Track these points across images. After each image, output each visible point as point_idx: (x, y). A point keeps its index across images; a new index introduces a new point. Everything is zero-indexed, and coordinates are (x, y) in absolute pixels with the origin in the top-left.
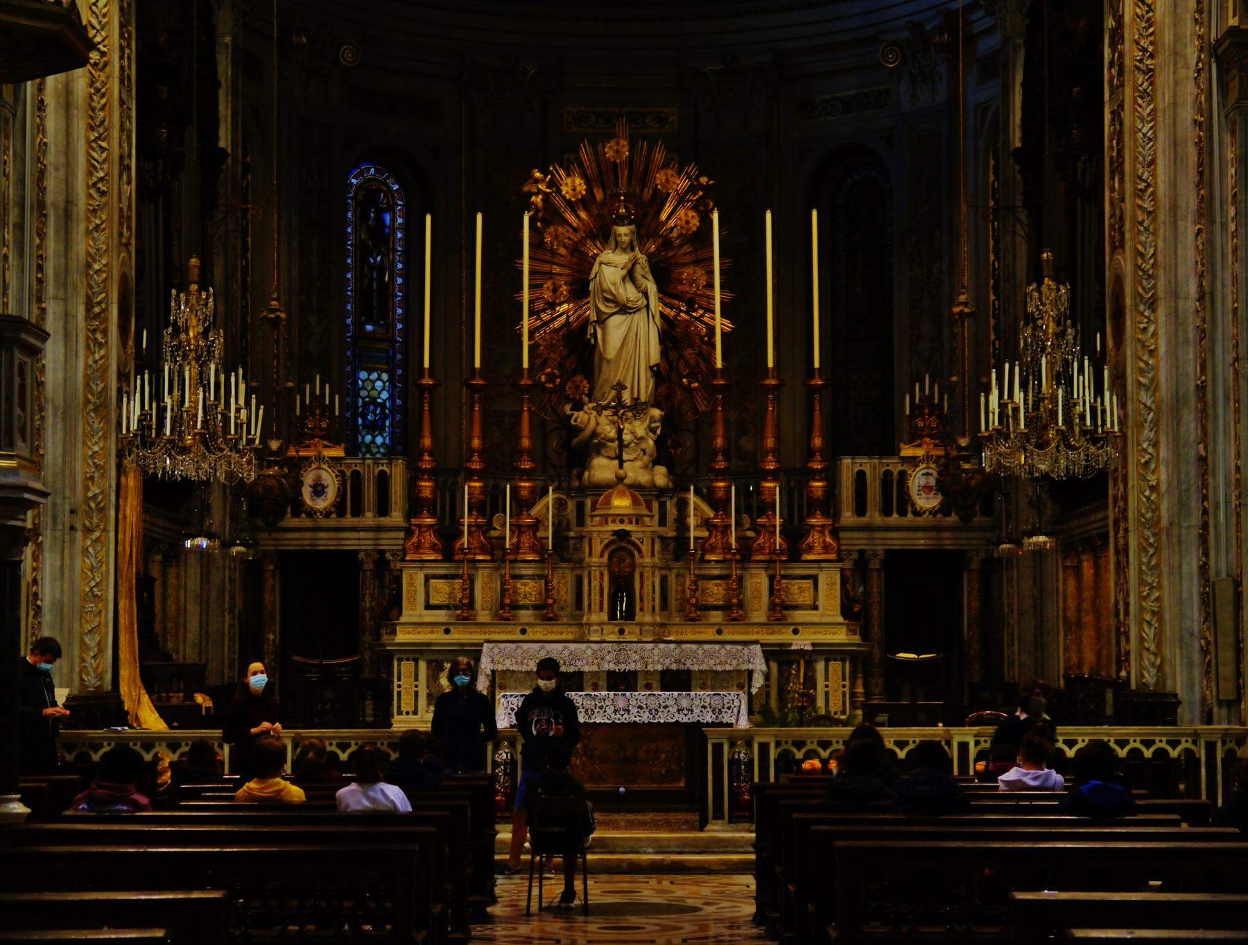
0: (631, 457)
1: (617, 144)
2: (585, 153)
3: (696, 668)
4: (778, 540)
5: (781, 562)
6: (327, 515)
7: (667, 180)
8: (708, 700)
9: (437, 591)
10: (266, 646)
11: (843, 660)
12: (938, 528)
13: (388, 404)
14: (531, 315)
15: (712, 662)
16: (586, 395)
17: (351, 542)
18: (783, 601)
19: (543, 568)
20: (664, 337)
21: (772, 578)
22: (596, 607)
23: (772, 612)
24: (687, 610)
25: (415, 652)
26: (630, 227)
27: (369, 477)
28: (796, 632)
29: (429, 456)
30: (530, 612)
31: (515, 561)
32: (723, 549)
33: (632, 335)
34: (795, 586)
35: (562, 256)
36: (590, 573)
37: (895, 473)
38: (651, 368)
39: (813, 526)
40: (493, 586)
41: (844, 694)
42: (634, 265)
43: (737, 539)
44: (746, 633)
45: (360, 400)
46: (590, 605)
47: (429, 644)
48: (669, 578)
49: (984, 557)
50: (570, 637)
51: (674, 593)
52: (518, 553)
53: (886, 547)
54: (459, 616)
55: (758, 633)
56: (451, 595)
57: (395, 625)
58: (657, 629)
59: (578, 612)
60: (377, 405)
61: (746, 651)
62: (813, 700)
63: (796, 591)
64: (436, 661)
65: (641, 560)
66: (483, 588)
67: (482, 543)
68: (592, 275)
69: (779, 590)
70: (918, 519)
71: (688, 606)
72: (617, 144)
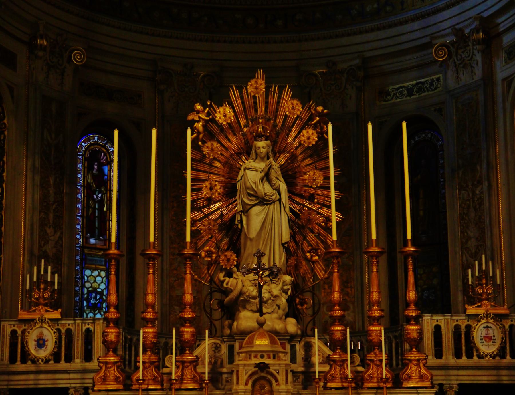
0: (269, 310)
1: (256, 82)
2: (234, 94)
6: (47, 361)
7: (293, 108)
12: (497, 368)
16: (235, 266)
20: (292, 224)
26: (266, 142)
27: (78, 334)
31: (180, 389)
32: (341, 378)
35: (217, 168)
37: (463, 327)
38: (283, 245)
39: (410, 361)
45: (86, 289)
52: (182, 383)
53: (459, 382)
60: (97, 293)
65: (278, 387)
68: (239, 178)
70: (482, 360)
72: (256, 82)
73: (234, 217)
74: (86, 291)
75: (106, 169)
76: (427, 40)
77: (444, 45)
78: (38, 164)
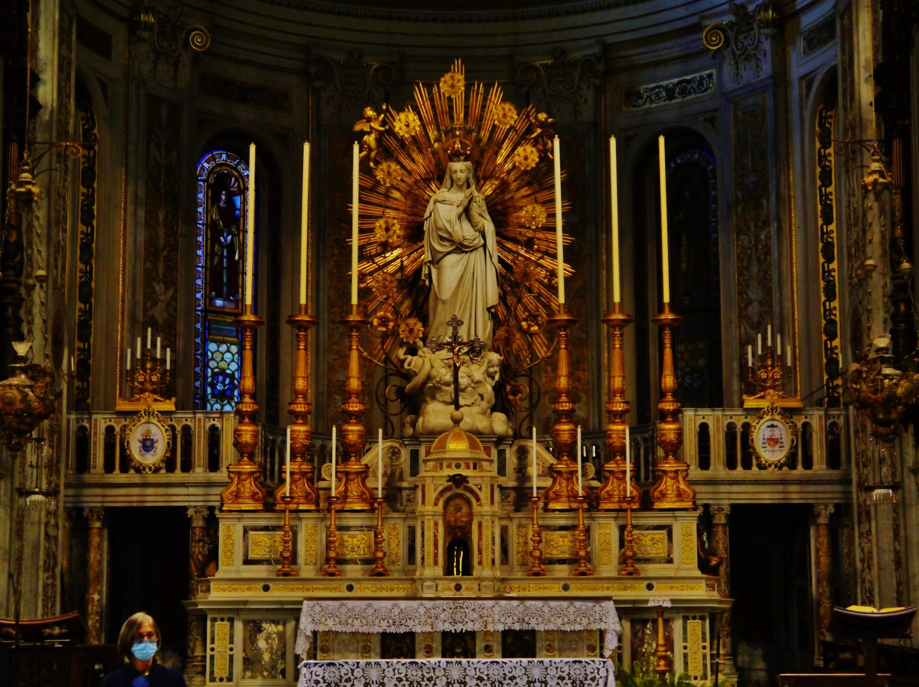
0: (469, 402)
1: (452, 78)
2: (420, 95)
3: (541, 628)
4: (629, 488)
5: (633, 510)
6: (157, 470)
8: (566, 669)
9: (257, 544)
10: (90, 608)
11: (703, 618)
12: (784, 482)
13: (236, 376)
14: (361, 259)
15: (559, 621)
17: (179, 498)
18: (635, 554)
19: (372, 518)
20: (501, 280)
21: (622, 528)
22: (429, 560)
23: (623, 566)
24: (531, 565)
25: (231, 612)
26: (465, 163)
27: (199, 432)
28: (650, 587)
29: (250, 398)
30: (358, 567)
31: (342, 511)
32: (569, 497)
33: (469, 276)
34: (647, 537)
35: (396, 199)
36: (423, 523)
38: (489, 309)
39: (665, 472)
40: (317, 538)
41: (704, 657)
42: (470, 202)
43: (583, 488)
44: (595, 589)
45: (209, 370)
46: (423, 558)
47: (245, 603)
48: (510, 530)
49: (833, 511)
50: (402, 594)
51: (515, 545)
52: (345, 502)
54: (279, 571)
55: (608, 589)
56: (272, 548)
57: (209, 581)
58: (498, 585)
59: (411, 567)
60: (226, 376)
61: (597, 608)
62: (670, 663)
63: (649, 542)
64: (254, 622)
65: (479, 509)
66: (307, 541)
67: (307, 492)
68: (427, 215)
69: (631, 542)
70: (764, 472)
71: (531, 559)
72: (452, 78)
73: (419, 271)
75: (238, 200)
76: (695, 19)
77: (718, 27)
78: (141, 193)
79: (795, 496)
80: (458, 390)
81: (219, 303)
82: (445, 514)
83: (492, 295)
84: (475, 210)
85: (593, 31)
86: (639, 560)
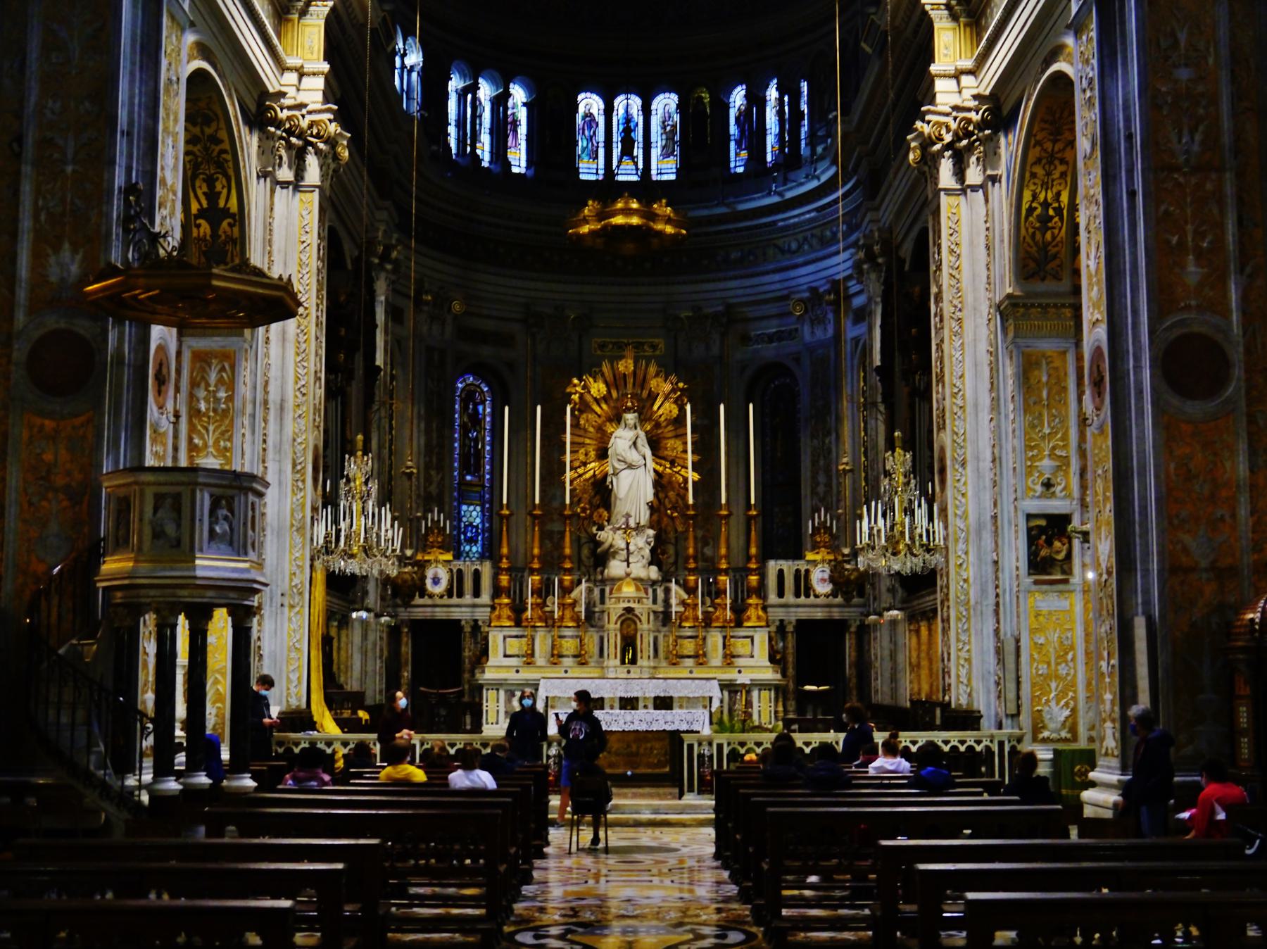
2: (606, 368)
6: (442, 597)
11: (770, 690)
14: (571, 470)
17: (456, 614)
21: (725, 638)
22: (612, 656)
33: (635, 484)
39: (750, 605)
43: (703, 613)
47: (506, 680)
50: (596, 675)
56: (520, 648)
58: (651, 670)
60: (473, 527)
73: (606, 475)
74: (463, 525)
75: (481, 408)
76: (785, 292)
77: (801, 300)
78: (422, 412)
79: (836, 614)
80: (629, 554)
81: (468, 478)
82: (621, 630)
83: (649, 493)
84: (639, 442)
85: (718, 294)
86: (734, 657)
